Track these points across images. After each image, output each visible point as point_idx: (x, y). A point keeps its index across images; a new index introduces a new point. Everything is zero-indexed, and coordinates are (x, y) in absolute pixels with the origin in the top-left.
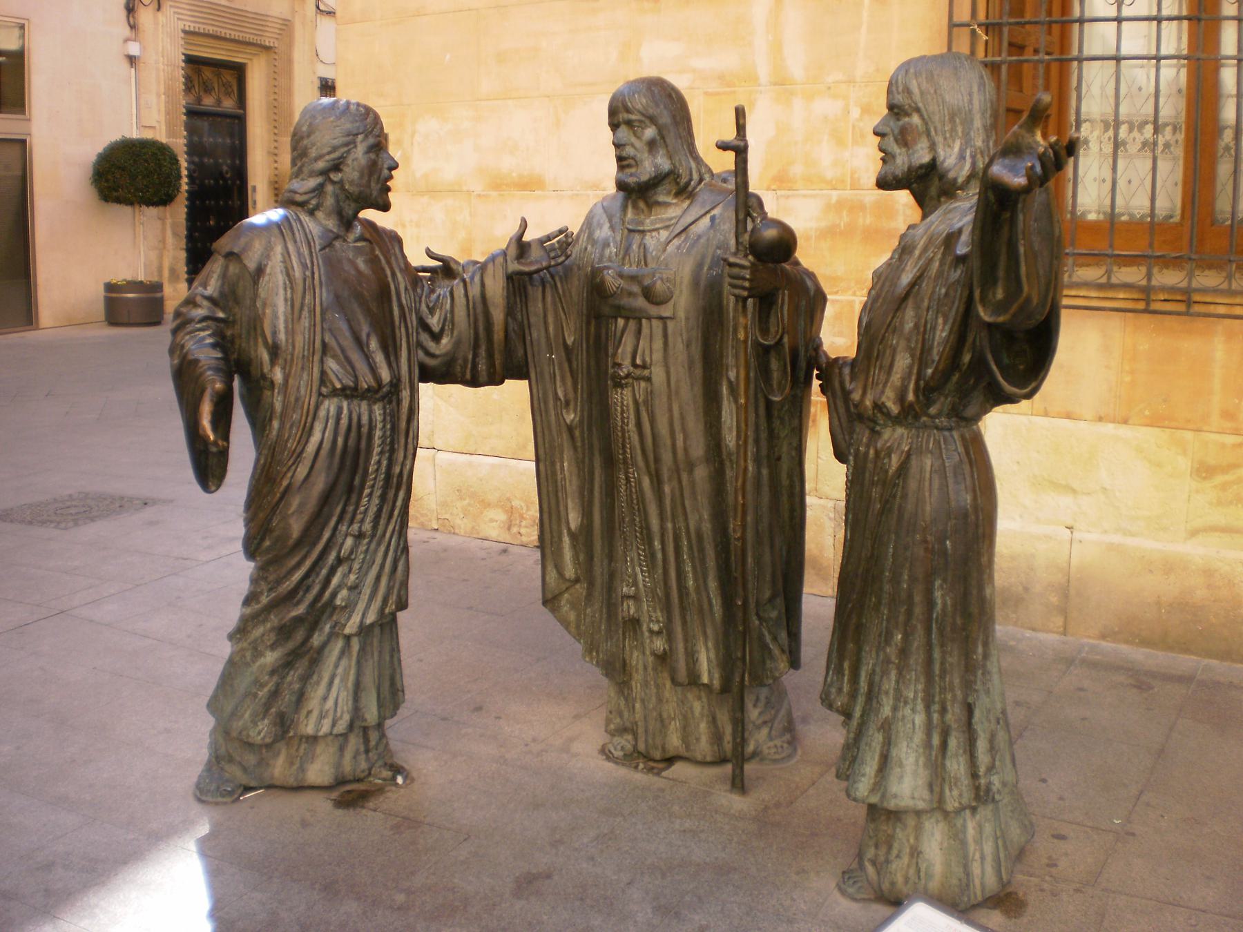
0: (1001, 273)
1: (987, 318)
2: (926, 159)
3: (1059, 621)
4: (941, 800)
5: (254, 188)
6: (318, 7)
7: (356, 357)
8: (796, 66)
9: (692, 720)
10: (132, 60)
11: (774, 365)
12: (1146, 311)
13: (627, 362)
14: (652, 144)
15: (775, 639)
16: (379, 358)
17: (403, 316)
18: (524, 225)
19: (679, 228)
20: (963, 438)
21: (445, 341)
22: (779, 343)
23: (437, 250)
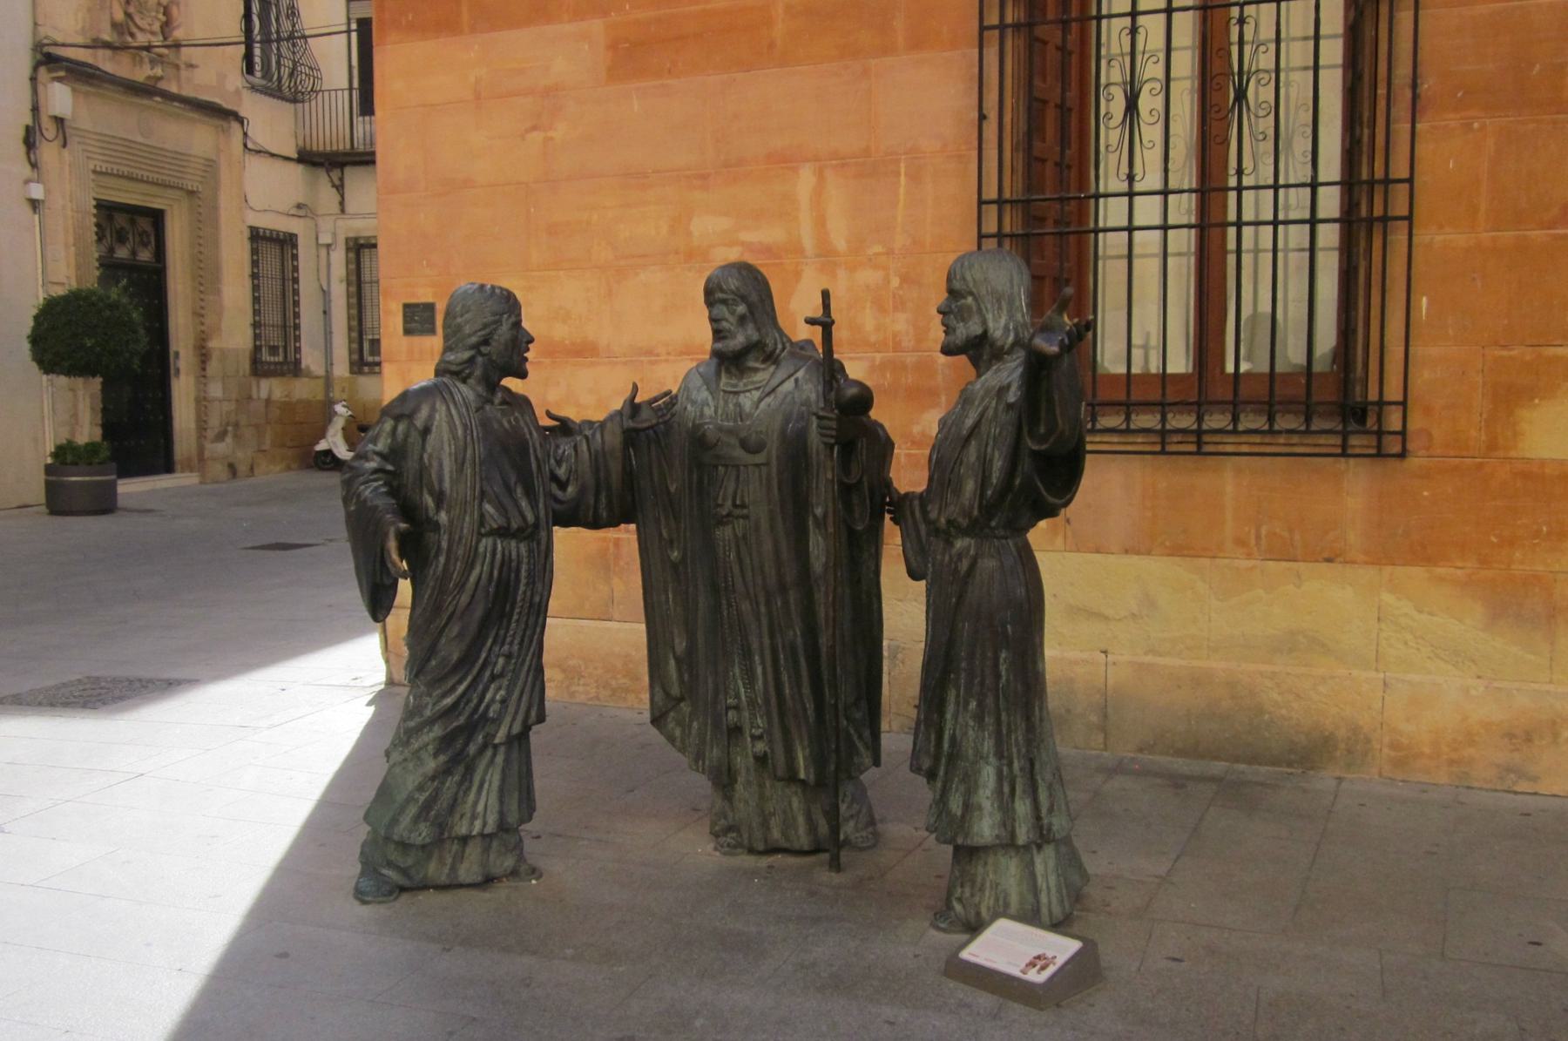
0: (1043, 414)
1: (1035, 447)
2: (978, 330)
3: (1101, 738)
4: (1013, 835)
5: (177, 354)
6: (245, 145)
7: (506, 501)
8: (840, 243)
9: (793, 813)
10: (35, 204)
11: (855, 500)
12: (1163, 452)
13: (729, 503)
14: (742, 320)
15: (860, 737)
16: (524, 503)
17: (539, 467)
18: (635, 388)
19: (768, 389)
20: (1015, 544)
21: (570, 489)
22: (860, 481)
23: (554, 411)
